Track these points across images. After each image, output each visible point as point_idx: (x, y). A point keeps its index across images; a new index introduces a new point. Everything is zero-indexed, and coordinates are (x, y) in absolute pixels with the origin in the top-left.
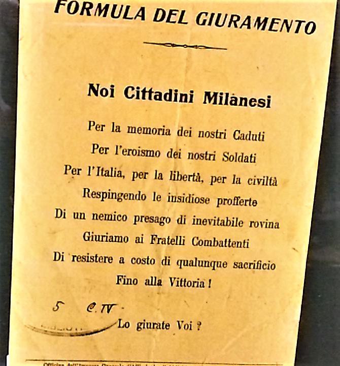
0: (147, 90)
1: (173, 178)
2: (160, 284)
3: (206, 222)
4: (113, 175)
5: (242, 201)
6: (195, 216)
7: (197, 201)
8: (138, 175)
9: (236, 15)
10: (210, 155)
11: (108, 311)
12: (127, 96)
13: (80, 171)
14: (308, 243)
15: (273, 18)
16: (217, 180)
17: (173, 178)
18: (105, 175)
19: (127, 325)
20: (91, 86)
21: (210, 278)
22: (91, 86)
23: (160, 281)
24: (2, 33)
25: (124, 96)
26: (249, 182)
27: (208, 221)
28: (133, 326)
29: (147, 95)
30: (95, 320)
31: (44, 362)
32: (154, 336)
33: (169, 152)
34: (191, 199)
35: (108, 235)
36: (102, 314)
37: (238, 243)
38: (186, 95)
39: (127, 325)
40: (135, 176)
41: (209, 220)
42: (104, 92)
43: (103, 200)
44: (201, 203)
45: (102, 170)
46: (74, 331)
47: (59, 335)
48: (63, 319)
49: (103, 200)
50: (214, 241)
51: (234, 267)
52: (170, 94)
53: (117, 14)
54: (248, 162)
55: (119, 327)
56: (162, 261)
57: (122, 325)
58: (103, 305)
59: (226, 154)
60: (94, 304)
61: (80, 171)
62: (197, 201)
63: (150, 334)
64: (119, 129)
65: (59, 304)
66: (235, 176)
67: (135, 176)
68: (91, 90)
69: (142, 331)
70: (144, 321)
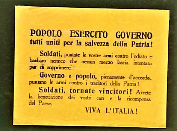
8: (67, 43)
10: (142, 44)
13: (72, 43)
14: (24, 6)
15: (109, 42)
16: (67, 43)
26: (70, 83)
35: (146, 43)
38: (53, 41)
40: (65, 44)
50: (92, 43)
52: (43, 34)
54: (138, 46)
56: (114, 44)
59: (42, 52)
61: (72, 43)
64: (126, 45)
66: (77, 41)
67: (65, 44)
70: (145, 42)
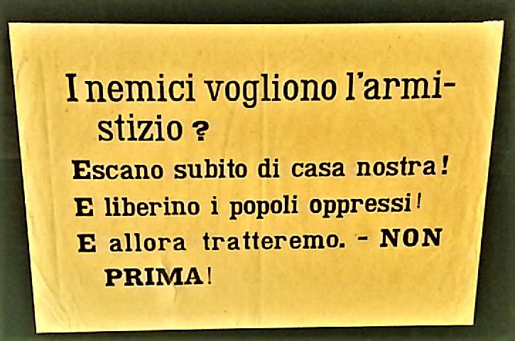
0: (251, 235)
1: (112, 211)
5: (267, 240)
7: (379, 171)
9: (372, 98)
17: (112, 211)
20: (436, 242)
21: (256, 231)
22: (436, 242)
24: (508, 152)
25: (100, 81)
29: (251, 241)
33: (261, 165)
34: (271, 87)
42: (150, 244)
44: (388, 173)
50: (208, 166)
51: (176, 177)
53: (291, 87)
58: (390, 98)
62: (379, 171)
68: (386, 237)
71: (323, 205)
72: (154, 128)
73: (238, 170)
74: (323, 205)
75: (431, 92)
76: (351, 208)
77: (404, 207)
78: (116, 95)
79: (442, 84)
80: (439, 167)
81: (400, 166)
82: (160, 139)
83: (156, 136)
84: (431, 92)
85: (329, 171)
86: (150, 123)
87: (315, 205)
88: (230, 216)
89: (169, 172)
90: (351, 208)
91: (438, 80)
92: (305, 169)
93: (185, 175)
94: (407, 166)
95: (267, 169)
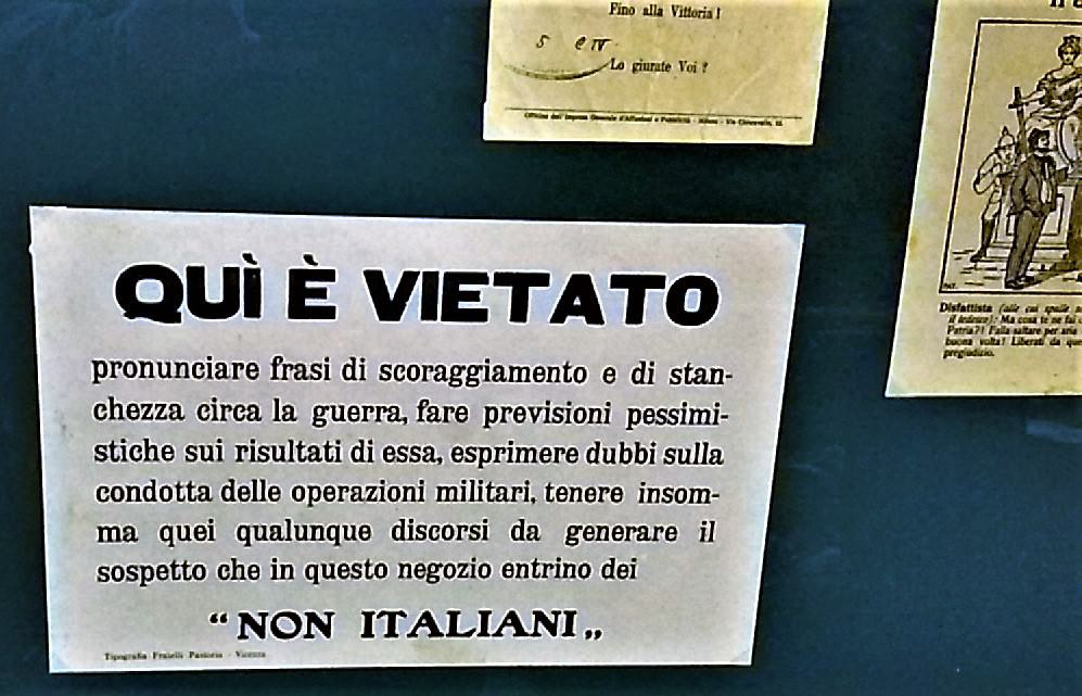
2: (660, 13)
3: (524, 413)
4: (700, 460)
6: (643, 484)
11: (600, 48)
12: (200, 417)
18: (497, 498)
19: (620, 67)
23: (661, 10)
27: (528, 412)
28: (628, 67)
30: (583, 60)
31: (525, 112)
32: (653, 80)
33: (346, 366)
36: (592, 53)
37: (551, 369)
39: (620, 67)
41: (531, 409)
43: (143, 585)
45: (489, 488)
46: (560, 74)
47: (545, 77)
48: (546, 59)
49: (143, 585)
55: (612, 68)
57: (615, 66)
60: (584, 39)
63: (648, 77)
64: (257, 412)
65: (545, 40)
69: (638, 74)
71: (307, 491)
72: (378, 491)
73: (581, 375)
74: (307, 491)
75: (712, 420)
76: (493, 458)
77: (680, 420)
78: (546, 458)
79: (720, 415)
80: (715, 14)
81: (364, 568)
82: (382, 500)
83: (379, 498)
84: (712, 420)
85: (419, 456)
86: (374, 488)
87: (274, 493)
88: (627, 426)
89: (180, 453)
90: (493, 458)
91: (717, 412)
92: (247, 413)
93: (268, 458)
94: (275, 567)
95: (352, 371)
